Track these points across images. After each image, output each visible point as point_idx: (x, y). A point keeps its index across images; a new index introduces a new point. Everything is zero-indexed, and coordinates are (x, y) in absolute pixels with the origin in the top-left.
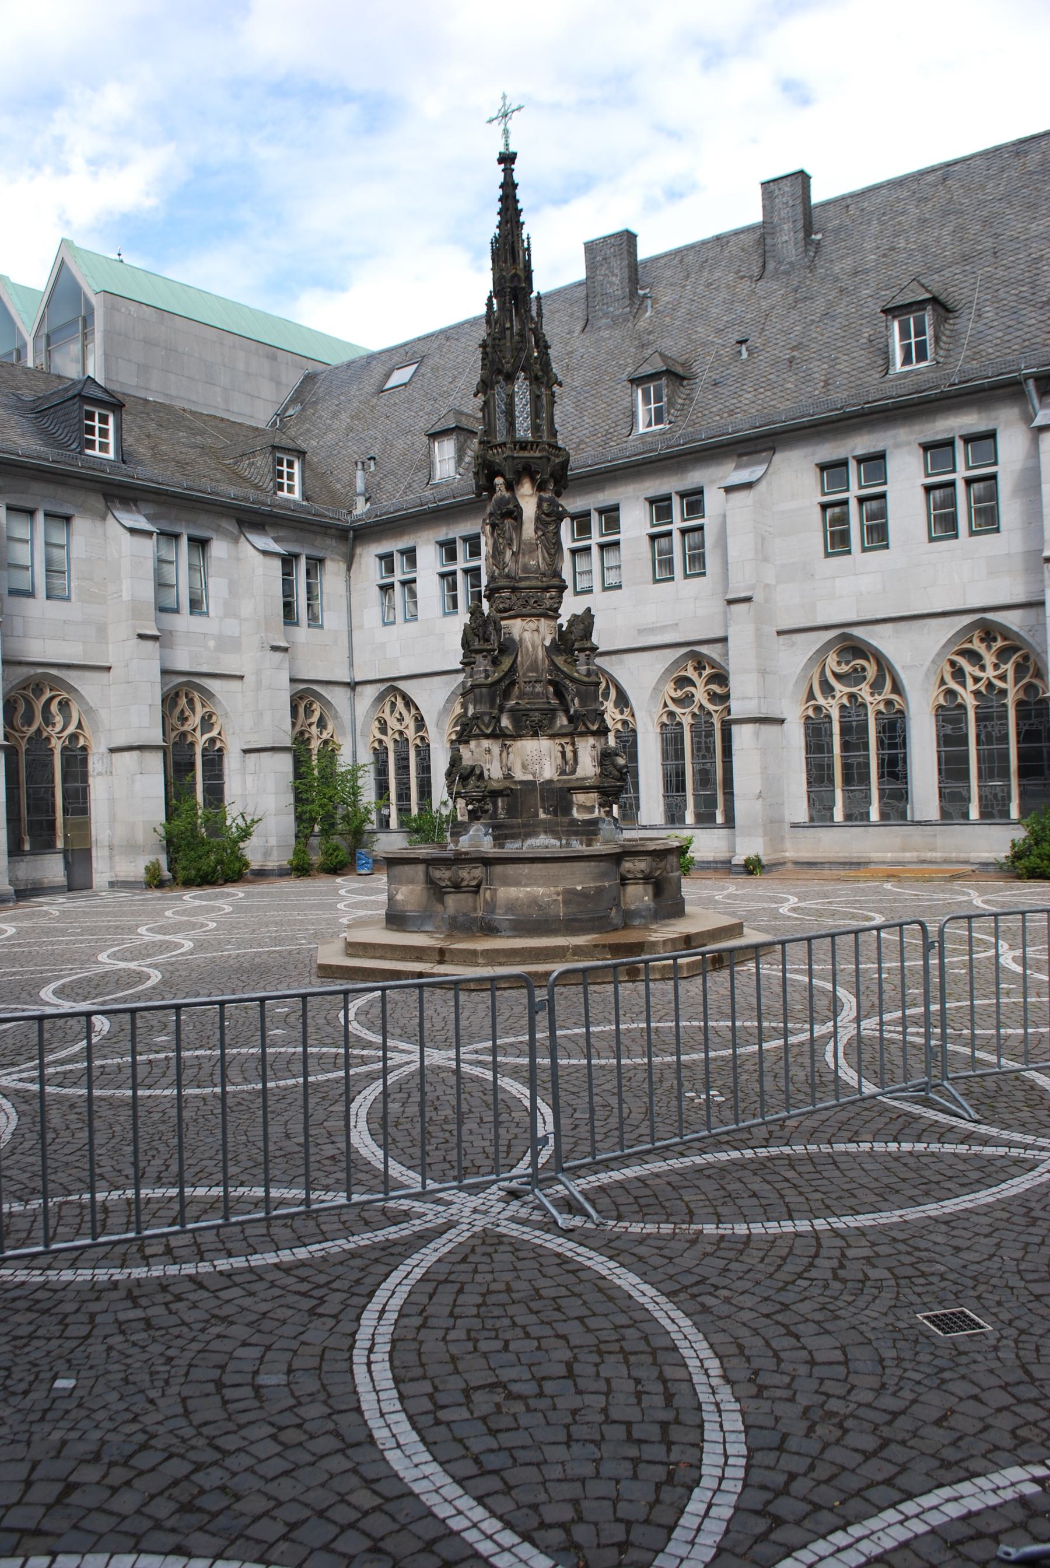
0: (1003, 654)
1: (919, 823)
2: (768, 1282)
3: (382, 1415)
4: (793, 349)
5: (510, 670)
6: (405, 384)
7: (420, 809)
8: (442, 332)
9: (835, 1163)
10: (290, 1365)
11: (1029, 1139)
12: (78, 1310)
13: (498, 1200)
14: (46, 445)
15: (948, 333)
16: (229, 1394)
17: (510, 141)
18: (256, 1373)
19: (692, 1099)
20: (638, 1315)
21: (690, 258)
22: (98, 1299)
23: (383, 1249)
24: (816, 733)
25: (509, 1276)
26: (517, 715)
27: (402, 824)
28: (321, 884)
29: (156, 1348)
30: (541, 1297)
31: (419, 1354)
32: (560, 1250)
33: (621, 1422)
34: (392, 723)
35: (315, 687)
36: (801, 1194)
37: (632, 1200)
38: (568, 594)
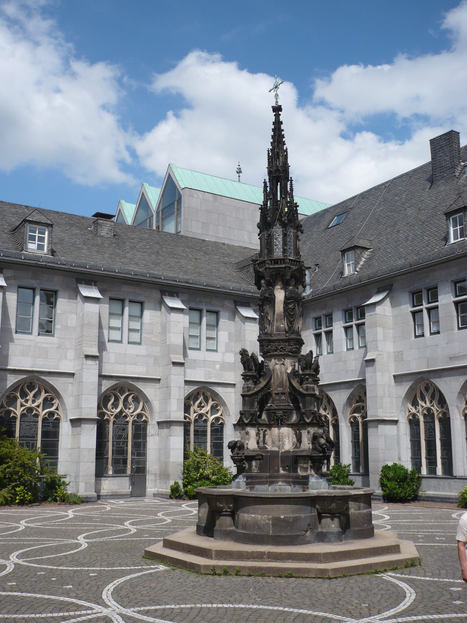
5: (265, 386)
17: (278, 100)
26: (270, 413)
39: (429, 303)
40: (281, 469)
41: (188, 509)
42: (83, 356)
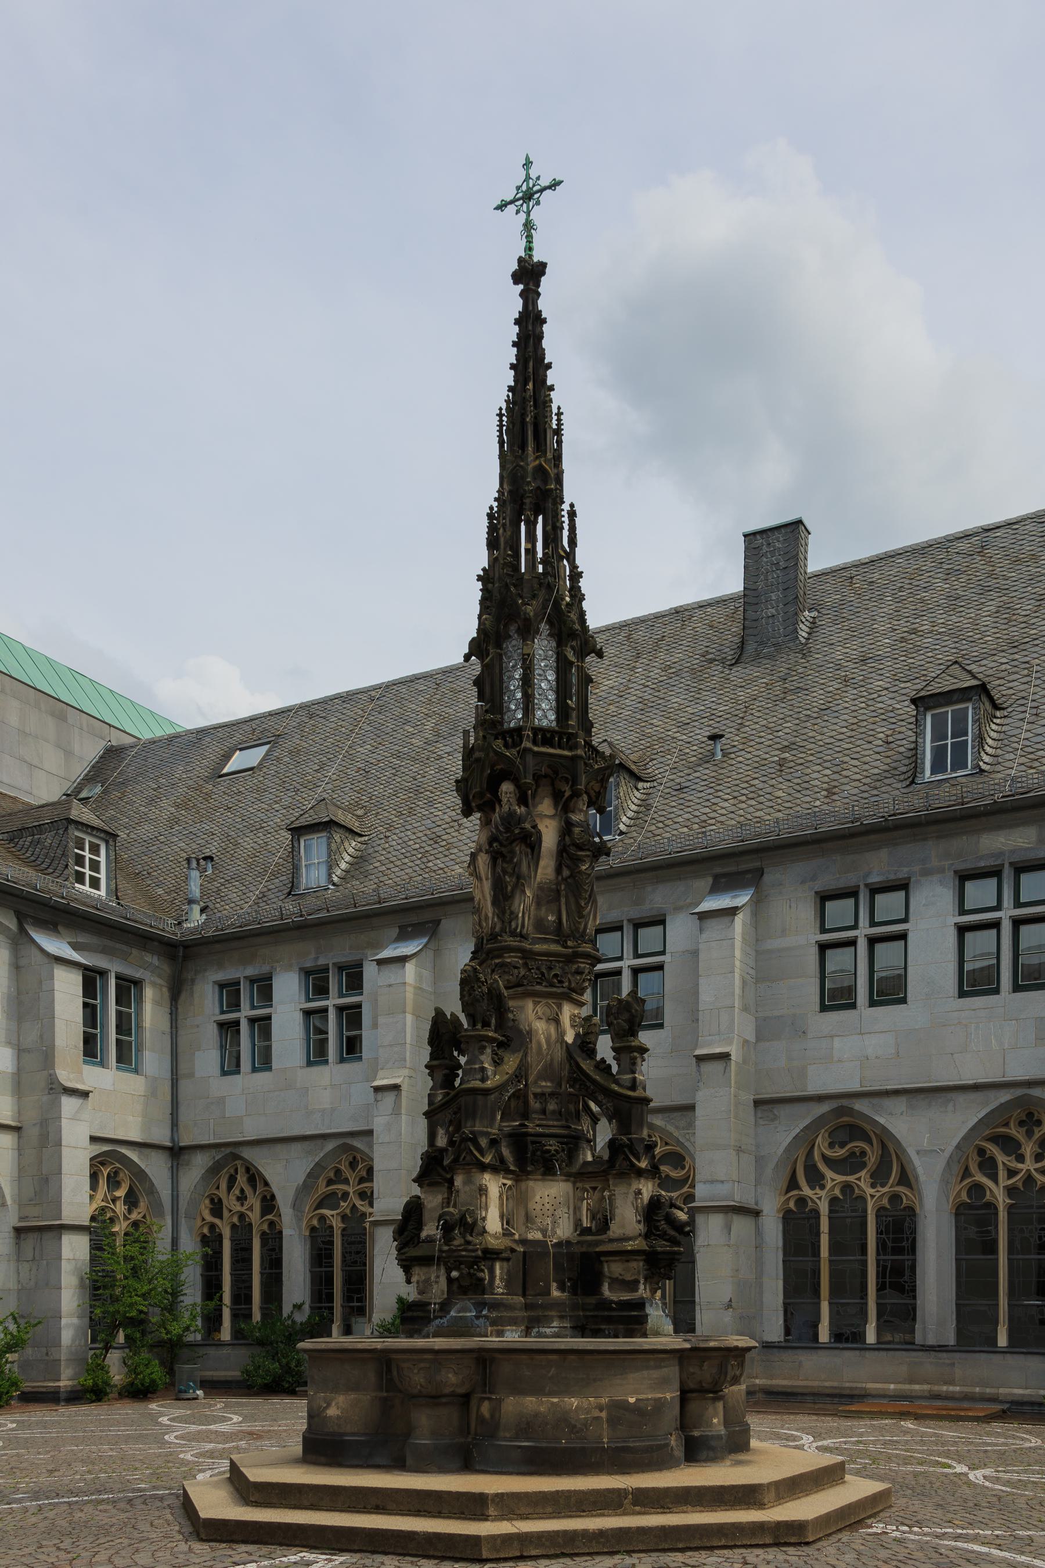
4: (784, 749)
6: (251, 769)
7: (264, 1316)
8: (303, 707)
15: (993, 734)
21: (640, 635)
24: (798, 1225)
27: (237, 1334)
28: (124, 1413)
34: (231, 1202)
40: (554, 1285)
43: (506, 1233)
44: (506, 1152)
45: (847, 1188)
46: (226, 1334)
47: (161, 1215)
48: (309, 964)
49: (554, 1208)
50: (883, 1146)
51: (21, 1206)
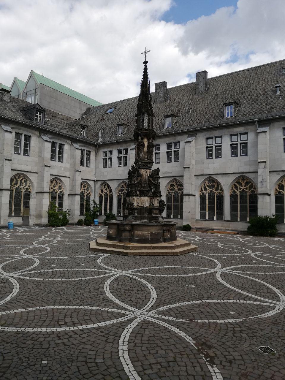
0: (247, 184)
1: (226, 221)
2: (217, 336)
3: (130, 372)
9: (225, 305)
10: (103, 357)
11: (271, 301)
12: (44, 340)
13: (146, 311)
14: (26, 119)
16: (90, 365)
18: (95, 359)
19: (187, 286)
20: (188, 344)
22: (49, 337)
23: (120, 324)
24: (203, 199)
25: (153, 332)
29: (67, 351)
30: (163, 339)
31: (136, 354)
32: (164, 325)
33: (192, 375)
34: (104, 190)
35: (86, 181)
36: (219, 313)
37: (179, 312)
38: (154, 164)
39: (156, 151)
41: (5, 234)
42: (3, 159)
43: (138, 205)
44: (138, 193)
45: (211, 191)
46: (103, 214)
47: (92, 192)
48: (119, 149)
49: (145, 201)
50: (218, 184)
51: (69, 191)
